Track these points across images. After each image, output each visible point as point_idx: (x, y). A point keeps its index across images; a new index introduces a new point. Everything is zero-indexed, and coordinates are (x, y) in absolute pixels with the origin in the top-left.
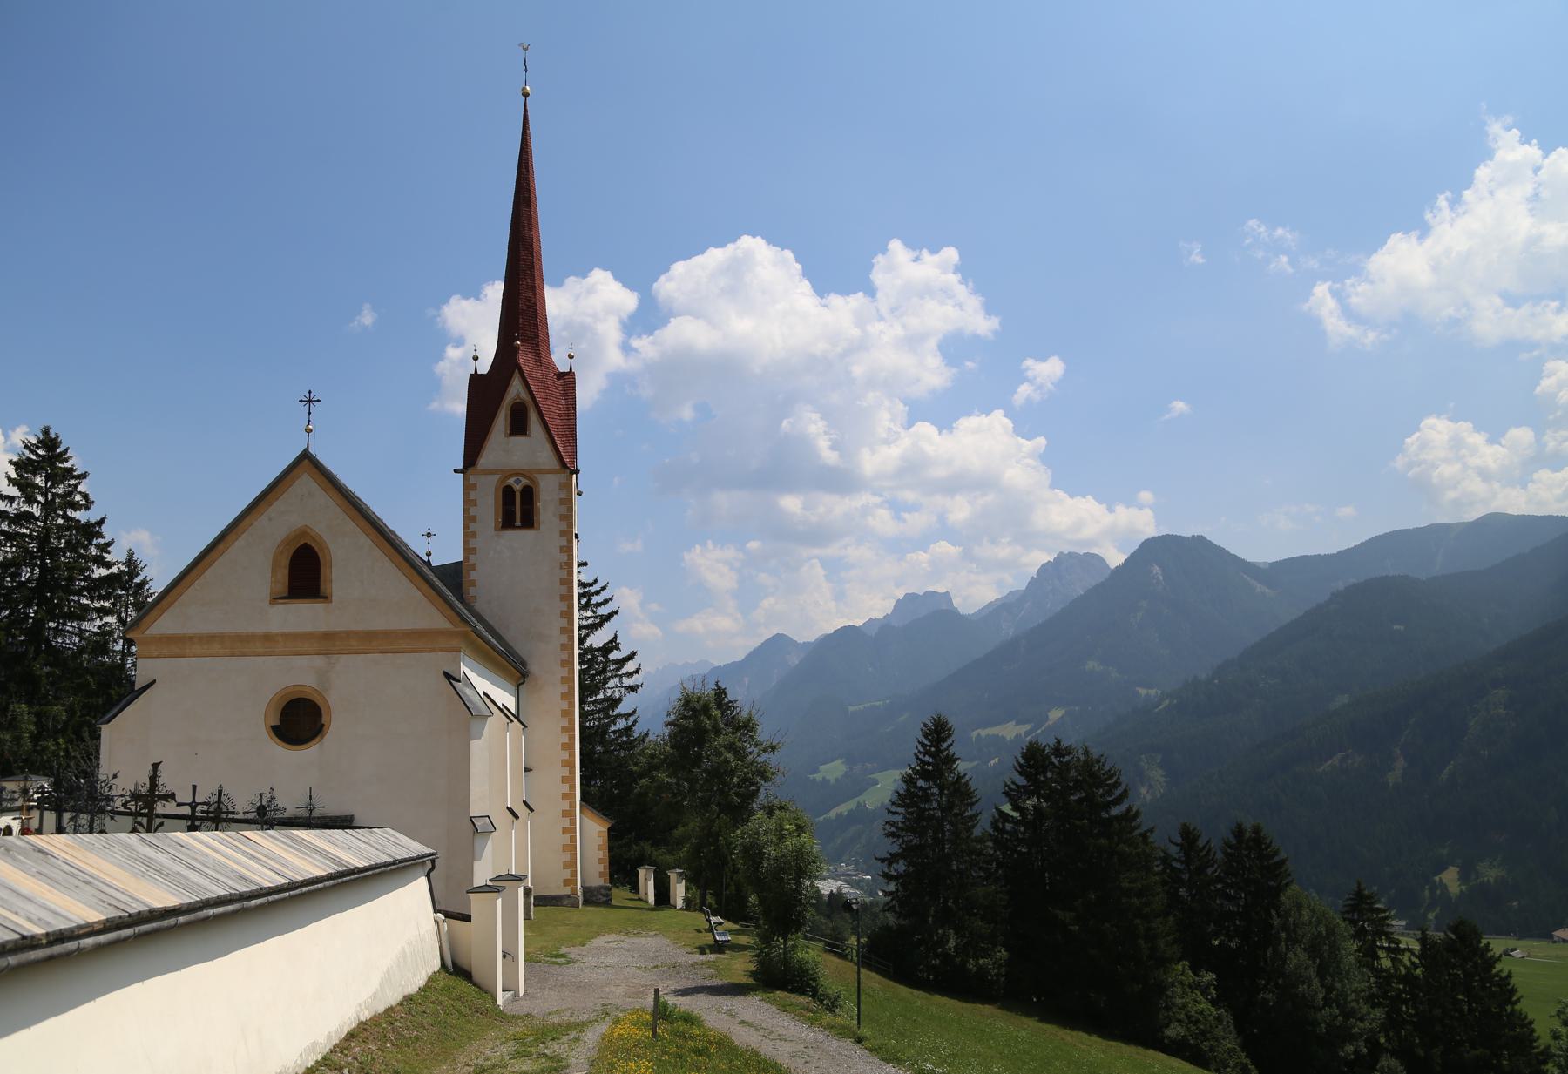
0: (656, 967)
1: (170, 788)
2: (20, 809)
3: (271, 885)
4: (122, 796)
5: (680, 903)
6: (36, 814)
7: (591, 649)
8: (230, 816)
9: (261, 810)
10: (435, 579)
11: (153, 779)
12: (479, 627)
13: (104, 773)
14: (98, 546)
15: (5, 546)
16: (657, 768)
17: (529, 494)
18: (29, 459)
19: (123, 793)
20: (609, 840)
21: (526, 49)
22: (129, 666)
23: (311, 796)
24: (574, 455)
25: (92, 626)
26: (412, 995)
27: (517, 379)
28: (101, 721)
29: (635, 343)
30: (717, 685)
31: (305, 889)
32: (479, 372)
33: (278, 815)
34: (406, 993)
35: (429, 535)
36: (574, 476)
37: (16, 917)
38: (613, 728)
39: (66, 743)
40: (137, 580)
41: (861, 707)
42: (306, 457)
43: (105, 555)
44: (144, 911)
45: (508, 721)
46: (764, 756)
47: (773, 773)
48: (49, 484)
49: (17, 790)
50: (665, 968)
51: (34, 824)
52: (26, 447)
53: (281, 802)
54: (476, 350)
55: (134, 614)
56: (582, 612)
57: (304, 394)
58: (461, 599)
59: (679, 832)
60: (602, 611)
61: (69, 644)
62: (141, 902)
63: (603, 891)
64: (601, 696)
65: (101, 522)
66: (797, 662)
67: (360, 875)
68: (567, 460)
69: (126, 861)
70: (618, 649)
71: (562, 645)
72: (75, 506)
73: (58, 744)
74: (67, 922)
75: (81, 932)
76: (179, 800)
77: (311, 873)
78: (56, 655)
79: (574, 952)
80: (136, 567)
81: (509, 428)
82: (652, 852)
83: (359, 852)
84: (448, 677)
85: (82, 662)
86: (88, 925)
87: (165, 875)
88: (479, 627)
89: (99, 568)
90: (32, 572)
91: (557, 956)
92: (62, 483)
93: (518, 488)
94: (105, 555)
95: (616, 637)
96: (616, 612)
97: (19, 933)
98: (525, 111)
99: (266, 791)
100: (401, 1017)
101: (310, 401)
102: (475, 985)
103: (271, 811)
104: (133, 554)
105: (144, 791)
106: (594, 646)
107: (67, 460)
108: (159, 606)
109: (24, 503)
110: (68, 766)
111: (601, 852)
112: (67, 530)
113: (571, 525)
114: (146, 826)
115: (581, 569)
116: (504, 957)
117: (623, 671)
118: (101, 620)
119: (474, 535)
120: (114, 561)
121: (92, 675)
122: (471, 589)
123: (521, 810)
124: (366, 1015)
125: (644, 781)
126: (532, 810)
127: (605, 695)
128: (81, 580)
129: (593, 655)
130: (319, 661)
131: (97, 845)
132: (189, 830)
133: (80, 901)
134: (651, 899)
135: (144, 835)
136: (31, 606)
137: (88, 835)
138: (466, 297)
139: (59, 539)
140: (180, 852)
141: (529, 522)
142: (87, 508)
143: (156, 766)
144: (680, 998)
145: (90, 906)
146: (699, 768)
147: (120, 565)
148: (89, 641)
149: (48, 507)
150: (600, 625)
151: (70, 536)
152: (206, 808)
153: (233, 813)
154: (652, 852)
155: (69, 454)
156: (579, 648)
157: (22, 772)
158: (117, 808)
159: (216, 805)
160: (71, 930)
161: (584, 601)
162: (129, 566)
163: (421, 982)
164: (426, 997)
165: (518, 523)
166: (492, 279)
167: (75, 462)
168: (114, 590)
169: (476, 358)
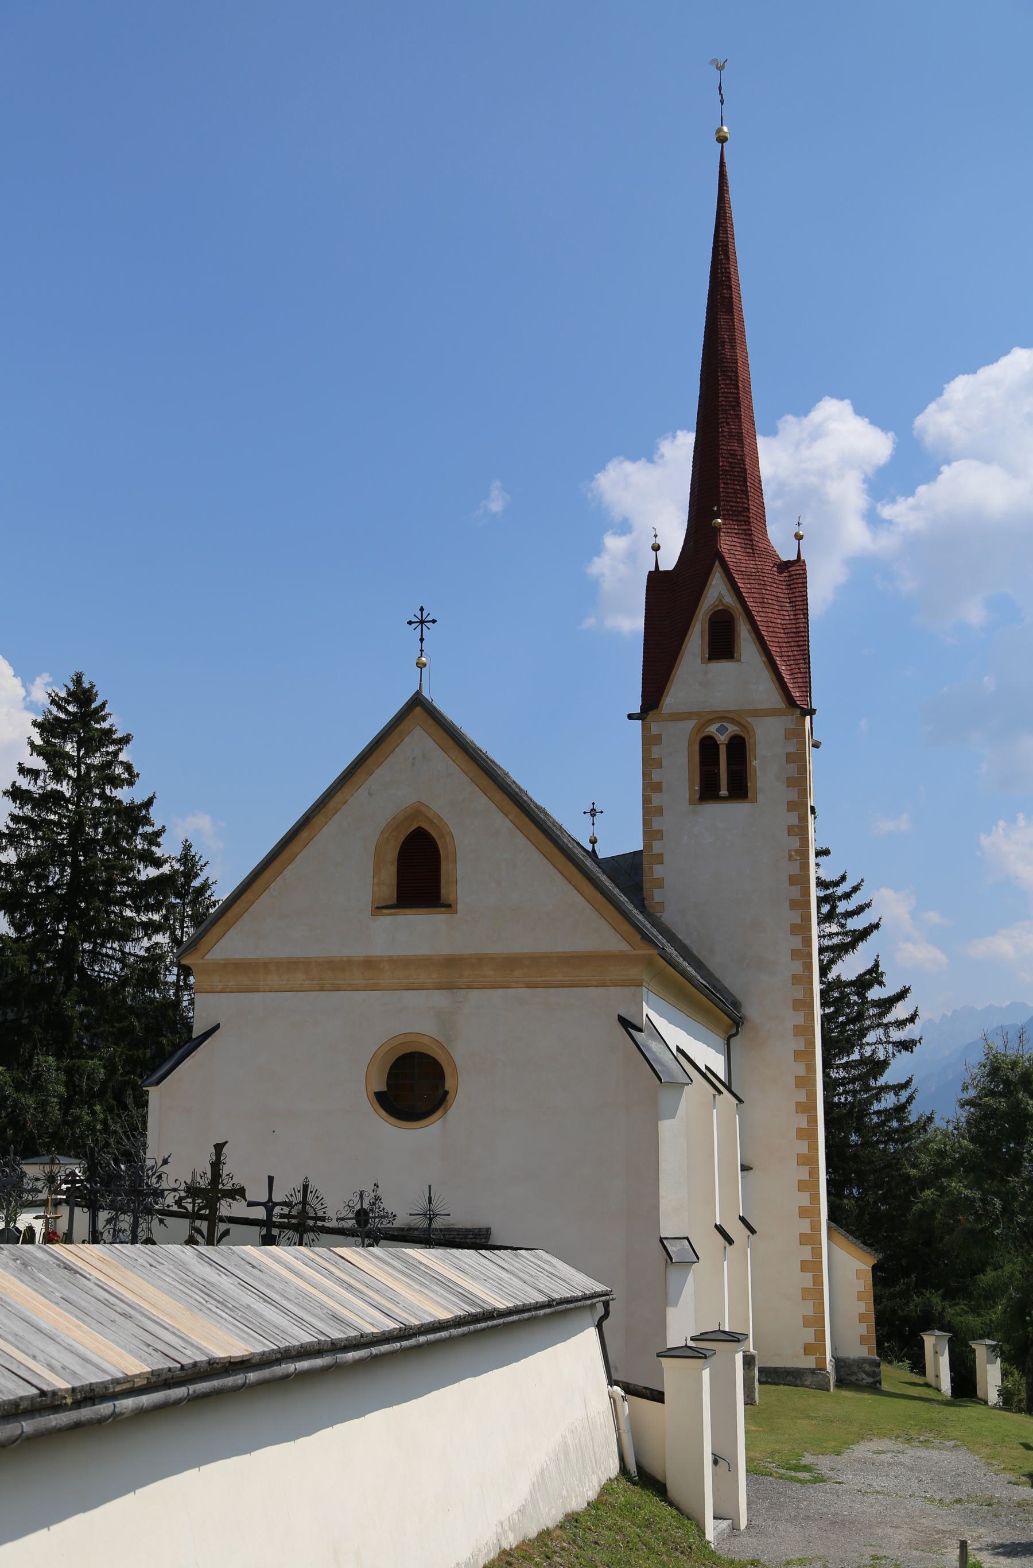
0: (959, 1501)
1: (238, 1180)
2: (44, 1203)
3: (375, 1331)
4: (175, 1190)
5: (993, 1397)
6: (64, 1211)
7: (838, 984)
8: (320, 1223)
9: (362, 1216)
10: (603, 878)
11: (216, 1166)
12: (671, 950)
13: (152, 1155)
14: (144, 836)
15: (28, 838)
16: (949, 1173)
17: (739, 748)
18: (57, 718)
19: (176, 1186)
20: (875, 1285)
21: (720, 68)
22: (185, 1004)
23: (430, 1198)
24: (806, 687)
25: (138, 948)
26: (578, 1514)
27: (718, 575)
28: (147, 1082)
29: (887, 512)
31: (422, 1339)
32: (661, 569)
33: (385, 1224)
34: (569, 1510)
35: (593, 813)
36: (808, 718)
37: (33, 1362)
38: (876, 1107)
39: (104, 1112)
40: (196, 883)
42: (418, 703)
43: (154, 849)
44: (202, 1362)
45: (715, 1092)
48: (82, 752)
49: (41, 1177)
50: (974, 1506)
51: (62, 1226)
52: (53, 702)
53: (389, 1205)
55: (191, 931)
56: (823, 926)
57: (413, 614)
58: (642, 907)
59: (987, 1278)
60: (855, 924)
61: (108, 973)
62: (198, 1348)
63: (867, 1367)
64: (855, 1056)
65: (149, 803)
67: (501, 1321)
68: (796, 694)
69: (177, 1285)
70: (881, 983)
71: (794, 976)
72: (116, 782)
73: (94, 1113)
74: (100, 1374)
75: (118, 1389)
76: (250, 1197)
77: (431, 1315)
78: (91, 984)
79: (824, 1463)
80: (193, 865)
81: (707, 651)
82: (943, 1309)
83: (500, 1286)
84: (627, 1024)
85: (125, 998)
86: (128, 1379)
87: (231, 1310)
88: (671, 950)
89: (146, 867)
90: (62, 875)
91: (797, 1468)
92: (98, 749)
93: (722, 739)
94: (154, 849)
95: (876, 965)
96: (876, 926)
97: (37, 1388)
98: (722, 164)
99: (368, 1188)
100: (563, 1549)
101: (422, 622)
102: (671, 1504)
103: (375, 1218)
104: (190, 846)
105: (204, 1183)
106: (843, 978)
107: (104, 718)
108: (223, 920)
109: (52, 778)
110: (107, 1144)
111: (862, 1304)
112: (105, 815)
113: (803, 793)
114: (205, 1233)
115: (822, 859)
116: (715, 1462)
117: (889, 1018)
118: (150, 939)
119: (659, 811)
120: (166, 856)
121: (138, 1017)
122: (656, 892)
123: (736, 1230)
124: (510, 1541)
125: (927, 1192)
126: (753, 1231)
127: (862, 1055)
128: (123, 884)
129: (842, 993)
130: (440, 999)
131: (140, 1261)
132: (264, 1244)
133: (117, 1343)
134: (946, 1385)
135: (202, 1248)
136: (59, 922)
137: (129, 1246)
138: (634, 458)
139: (95, 827)
140: (250, 1274)
141: (740, 790)
142: (131, 783)
143: (219, 1148)
144: (1001, 1559)
145: (130, 1352)
146: (1017, 1175)
147: (174, 863)
148: (134, 969)
149: (81, 784)
150: (853, 945)
151: (110, 823)
152: (286, 1210)
153: (323, 1219)
154: (943, 1309)
155: (107, 710)
156: (822, 982)
157: (49, 1152)
158: (168, 1206)
159: (300, 1206)
160: (104, 1385)
161: (826, 909)
162: (185, 864)
163: (590, 1494)
164: (598, 1518)
165: (724, 792)
166: (670, 430)
167: (116, 721)
168: (166, 897)
169: (656, 548)
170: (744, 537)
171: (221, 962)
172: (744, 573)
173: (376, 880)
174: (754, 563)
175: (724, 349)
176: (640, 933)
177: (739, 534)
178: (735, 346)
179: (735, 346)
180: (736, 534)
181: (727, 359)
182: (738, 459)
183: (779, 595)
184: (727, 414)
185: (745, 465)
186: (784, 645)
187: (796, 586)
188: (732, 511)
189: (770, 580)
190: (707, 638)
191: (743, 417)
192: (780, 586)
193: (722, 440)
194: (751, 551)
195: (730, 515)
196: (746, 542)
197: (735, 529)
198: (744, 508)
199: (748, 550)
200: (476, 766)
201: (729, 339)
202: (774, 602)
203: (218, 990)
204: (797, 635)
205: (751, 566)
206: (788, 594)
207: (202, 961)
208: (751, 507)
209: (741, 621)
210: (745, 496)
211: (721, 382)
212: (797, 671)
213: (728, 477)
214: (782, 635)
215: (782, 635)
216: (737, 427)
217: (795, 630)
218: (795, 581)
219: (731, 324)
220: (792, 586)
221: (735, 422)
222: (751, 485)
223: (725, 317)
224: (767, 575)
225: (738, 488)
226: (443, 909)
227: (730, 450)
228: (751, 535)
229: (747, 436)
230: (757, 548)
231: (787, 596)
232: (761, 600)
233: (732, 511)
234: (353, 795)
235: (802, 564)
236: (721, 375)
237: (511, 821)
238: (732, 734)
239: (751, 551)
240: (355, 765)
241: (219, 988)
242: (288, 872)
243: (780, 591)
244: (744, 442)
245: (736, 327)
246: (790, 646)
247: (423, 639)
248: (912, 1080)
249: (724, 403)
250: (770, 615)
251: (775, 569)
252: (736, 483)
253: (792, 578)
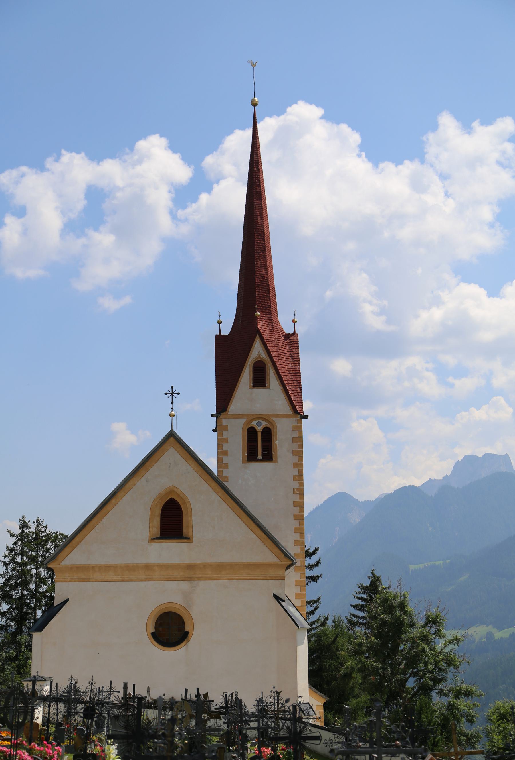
17: (268, 433)
21: (254, 66)
30: (373, 574)
32: (222, 334)
41: (422, 566)
42: (172, 435)
46: (450, 647)
47: (460, 662)
54: (219, 316)
57: (167, 390)
66: (358, 520)
93: (259, 429)
101: (172, 394)
108: (70, 544)
130: (185, 585)
141: (268, 457)
165: (260, 457)
169: (220, 323)
170: (268, 321)
171: (69, 566)
172: (269, 341)
173: (151, 525)
174: (273, 335)
175: (257, 219)
176: (284, 554)
177: (266, 319)
178: (263, 218)
179: (263, 218)
180: (264, 319)
181: (258, 224)
182: (265, 279)
183: (286, 352)
184: (259, 254)
185: (268, 282)
186: (290, 380)
187: (294, 348)
188: (262, 307)
189: (281, 344)
190: (252, 375)
191: (267, 256)
192: (286, 348)
193: (257, 268)
194: (272, 329)
195: (261, 309)
196: (269, 324)
197: (264, 317)
198: (268, 305)
199: (270, 328)
200: (202, 468)
201: (260, 214)
202: (284, 357)
203: (68, 581)
204: (296, 375)
205: (272, 337)
206: (290, 352)
207: (59, 566)
208: (272, 305)
209: (270, 368)
210: (268, 299)
211: (256, 237)
212: (297, 394)
213: (260, 288)
214: (288, 375)
215: (288, 375)
216: (264, 262)
217: (294, 372)
218: (293, 345)
219: (260, 206)
220: (292, 348)
221: (263, 259)
222: (271, 293)
223: (258, 202)
224: (279, 342)
225: (265, 294)
226: (186, 540)
227: (261, 274)
228: (271, 320)
229: (269, 267)
230: (275, 327)
231: (289, 353)
232: (278, 355)
233: (262, 307)
234: (138, 481)
235: (296, 336)
236: (256, 234)
237: (220, 497)
238: (265, 426)
239: (272, 329)
240: (140, 466)
241: (68, 580)
242: (104, 520)
243: (286, 350)
244: (268, 270)
245: (263, 208)
246: (293, 381)
247: (173, 403)
248: (320, 598)
249: (257, 248)
250: (282, 363)
251: (283, 338)
252: (264, 292)
253: (291, 343)
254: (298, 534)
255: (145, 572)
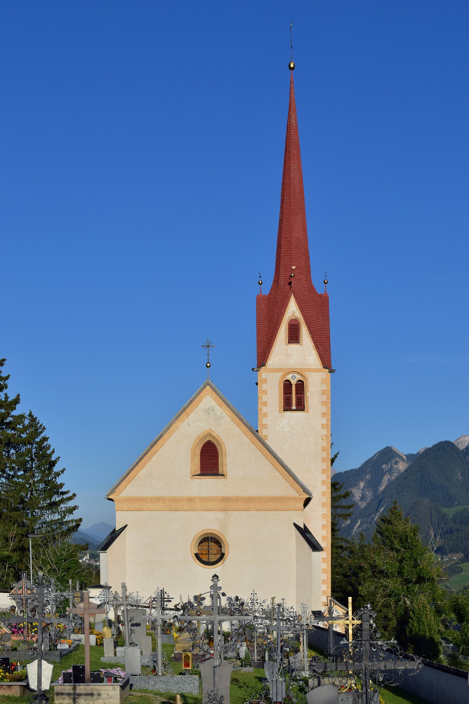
17: (301, 386)
54: (260, 277)
93: (294, 382)
130: (220, 515)
141: (301, 406)
165: (294, 407)
171: (126, 498)
173: (192, 463)
203: (126, 510)
207: (118, 497)
209: (303, 325)
241: (126, 509)
254: (325, 475)
255: (188, 503)
